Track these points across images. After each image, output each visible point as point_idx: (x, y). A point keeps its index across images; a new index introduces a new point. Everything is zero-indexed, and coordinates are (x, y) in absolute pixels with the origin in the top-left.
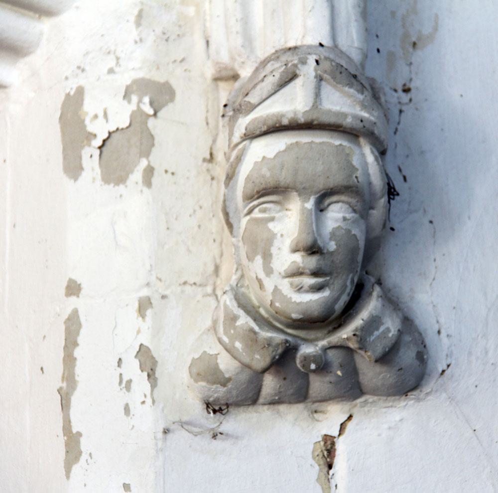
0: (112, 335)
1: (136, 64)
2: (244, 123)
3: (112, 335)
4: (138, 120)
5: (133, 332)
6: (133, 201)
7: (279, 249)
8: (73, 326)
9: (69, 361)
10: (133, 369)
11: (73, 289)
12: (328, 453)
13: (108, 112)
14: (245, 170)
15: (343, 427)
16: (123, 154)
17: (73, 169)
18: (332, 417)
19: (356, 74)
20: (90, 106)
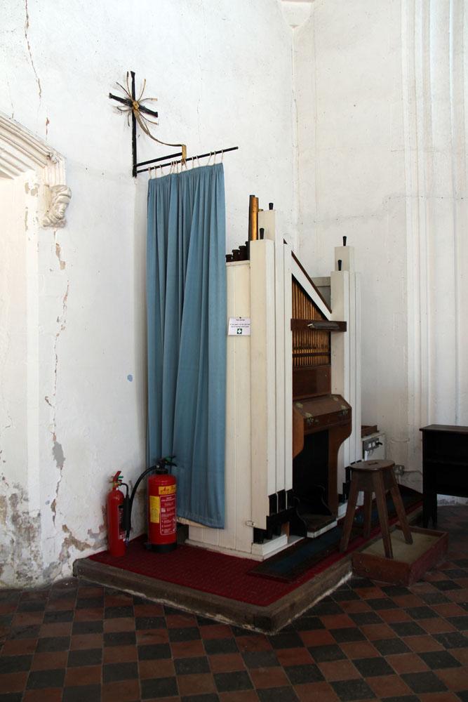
0: (32, 215)
1: (36, 181)
2: (60, 193)
3: (32, 215)
4: (36, 188)
5: (36, 215)
6: (35, 198)
7: (101, 216)
8: (27, 213)
9: (26, 217)
10: (35, 219)
11: (27, 208)
12: (55, 232)
13: (32, 187)
14: (58, 199)
15: (222, 158)
16: (34, 192)
17: (27, 192)
18: (55, 229)
19: (414, 541)
20: (29, 185)
